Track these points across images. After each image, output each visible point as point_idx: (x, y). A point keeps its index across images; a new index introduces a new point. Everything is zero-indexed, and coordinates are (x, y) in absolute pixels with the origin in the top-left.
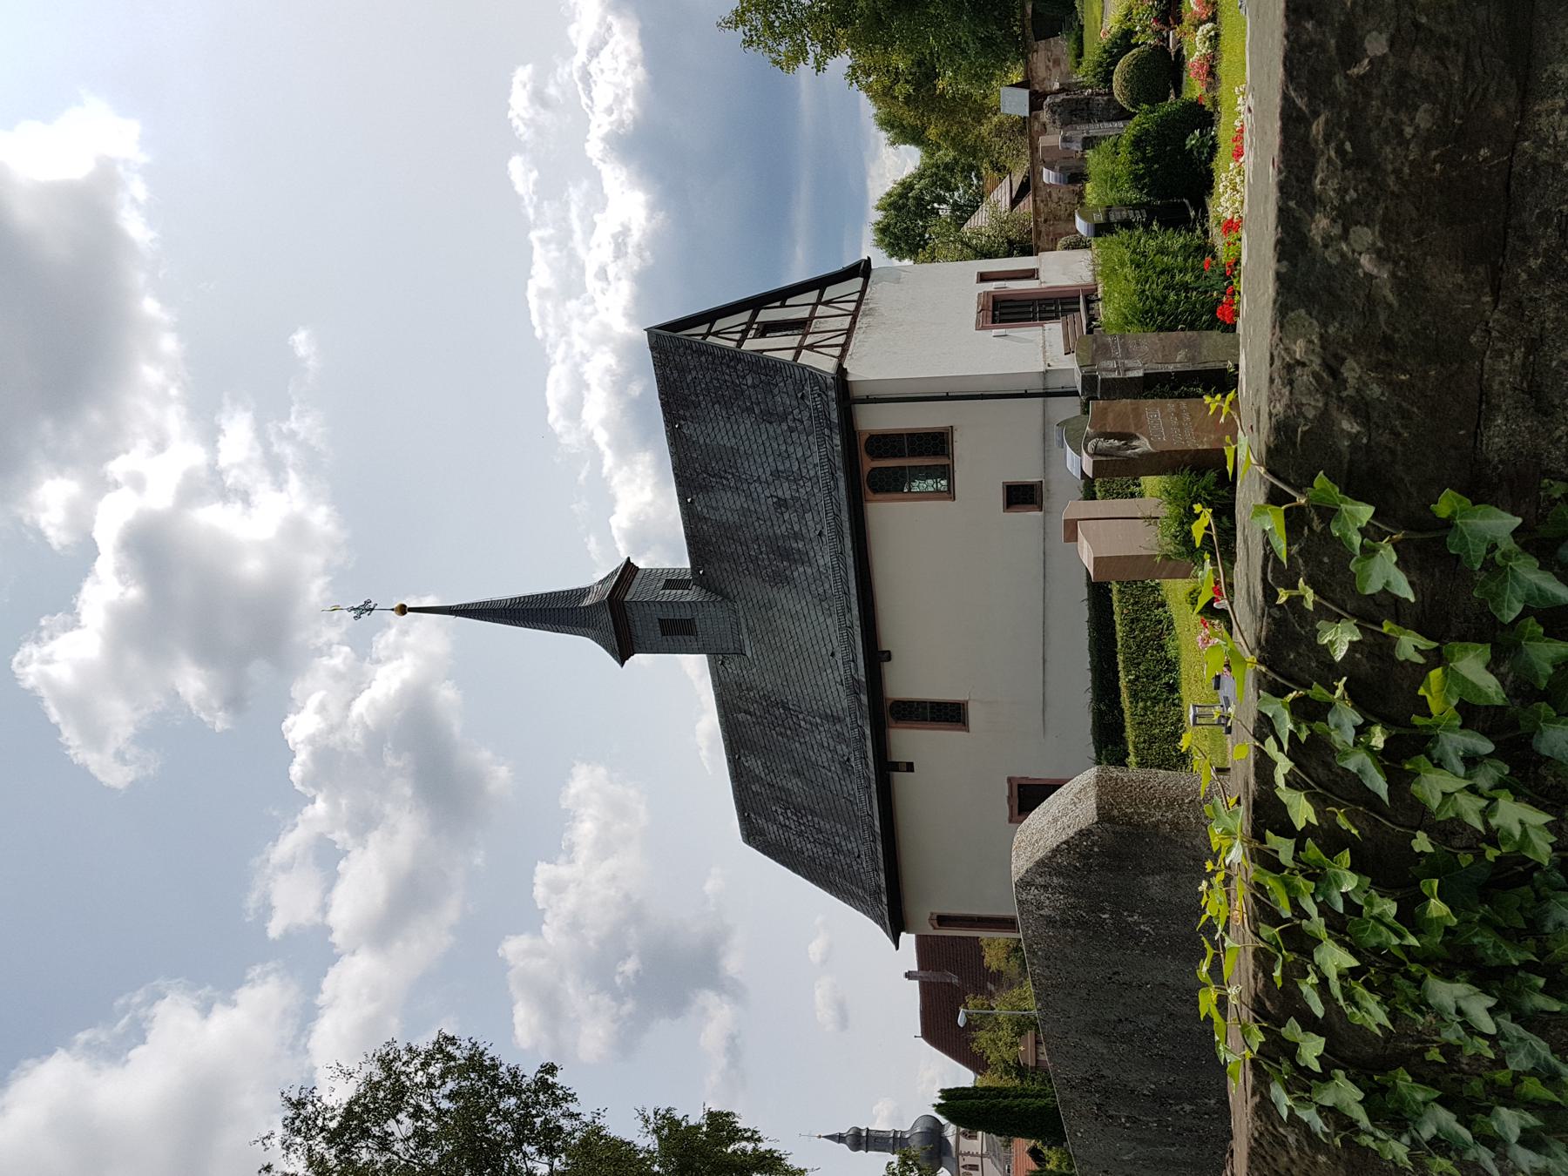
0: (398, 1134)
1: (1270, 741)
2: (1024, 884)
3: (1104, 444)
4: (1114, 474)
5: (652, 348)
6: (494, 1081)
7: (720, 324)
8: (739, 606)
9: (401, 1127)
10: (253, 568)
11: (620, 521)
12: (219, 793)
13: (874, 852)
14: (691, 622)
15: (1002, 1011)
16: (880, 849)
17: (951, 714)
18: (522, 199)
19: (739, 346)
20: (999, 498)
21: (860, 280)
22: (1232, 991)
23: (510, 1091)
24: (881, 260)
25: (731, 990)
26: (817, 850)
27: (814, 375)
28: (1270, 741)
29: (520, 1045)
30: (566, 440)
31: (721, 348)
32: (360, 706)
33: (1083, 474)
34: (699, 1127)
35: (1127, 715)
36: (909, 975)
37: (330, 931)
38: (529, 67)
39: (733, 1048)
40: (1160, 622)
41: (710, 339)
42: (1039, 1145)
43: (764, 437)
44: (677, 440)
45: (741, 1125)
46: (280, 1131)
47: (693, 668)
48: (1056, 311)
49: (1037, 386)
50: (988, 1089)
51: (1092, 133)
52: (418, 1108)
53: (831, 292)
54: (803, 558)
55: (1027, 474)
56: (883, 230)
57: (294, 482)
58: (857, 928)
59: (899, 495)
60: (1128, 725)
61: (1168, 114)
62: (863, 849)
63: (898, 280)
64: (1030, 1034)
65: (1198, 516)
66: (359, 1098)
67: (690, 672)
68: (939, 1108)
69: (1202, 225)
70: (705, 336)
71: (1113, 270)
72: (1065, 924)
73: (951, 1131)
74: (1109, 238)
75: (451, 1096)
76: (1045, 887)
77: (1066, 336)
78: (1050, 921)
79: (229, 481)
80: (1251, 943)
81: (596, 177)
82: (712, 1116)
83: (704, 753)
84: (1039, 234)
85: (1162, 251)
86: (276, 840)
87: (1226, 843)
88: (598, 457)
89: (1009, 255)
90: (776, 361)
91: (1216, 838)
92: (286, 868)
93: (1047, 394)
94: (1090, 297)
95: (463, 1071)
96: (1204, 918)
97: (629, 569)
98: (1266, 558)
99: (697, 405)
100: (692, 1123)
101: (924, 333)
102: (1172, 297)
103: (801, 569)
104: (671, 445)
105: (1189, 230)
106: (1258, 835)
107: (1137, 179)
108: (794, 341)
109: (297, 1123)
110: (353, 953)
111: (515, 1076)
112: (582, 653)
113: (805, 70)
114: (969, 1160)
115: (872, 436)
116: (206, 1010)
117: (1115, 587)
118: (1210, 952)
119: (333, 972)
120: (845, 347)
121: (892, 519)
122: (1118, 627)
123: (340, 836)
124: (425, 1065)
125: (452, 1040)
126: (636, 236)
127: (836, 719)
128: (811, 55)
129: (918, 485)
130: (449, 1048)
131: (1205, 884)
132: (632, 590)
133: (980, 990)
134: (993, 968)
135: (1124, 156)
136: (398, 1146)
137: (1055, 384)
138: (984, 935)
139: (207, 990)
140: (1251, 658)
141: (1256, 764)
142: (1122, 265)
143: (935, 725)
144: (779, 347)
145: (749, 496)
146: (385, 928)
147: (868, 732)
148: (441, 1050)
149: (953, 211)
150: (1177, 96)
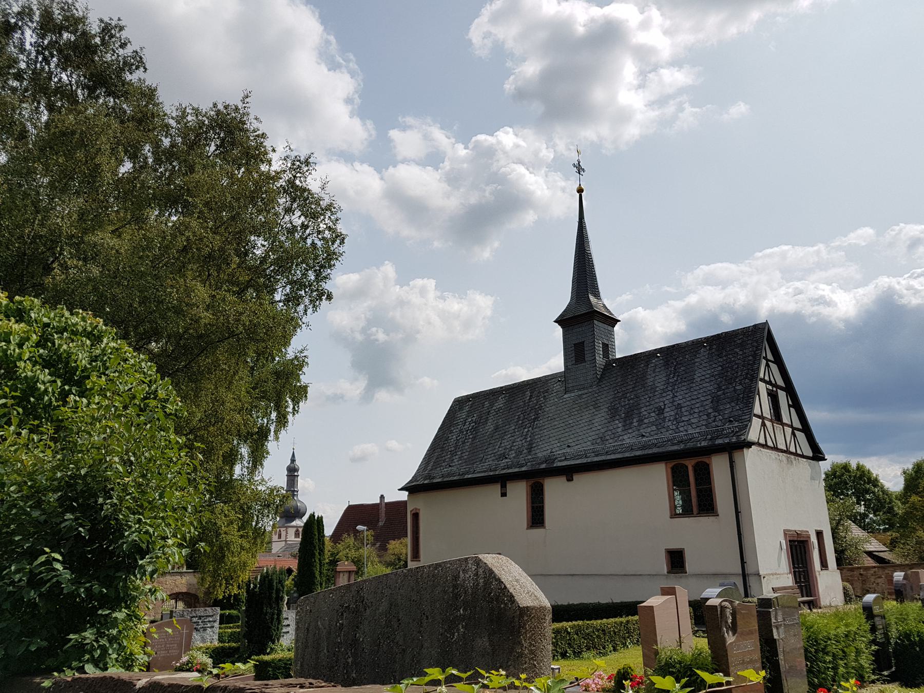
0: (293, 217)
2: (478, 562)
3: (728, 612)
5: (755, 326)
6: (322, 267)
7: (774, 367)
8: (595, 388)
9: (297, 219)
10: (598, 95)
11: (641, 313)
12: (470, 97)
13: (453, 475)
15: (366, 551)
16: (455, 478)
17: (537, 518)
18: (846, 236)
21: (811, 454)
23: (317, 276)
24: (825, 466)
25: (368, 395)
26: (452, 441)
27: (746, 427)
29: (340, 280)
31: (758, 369)
32: (521, 169)
33: (707, 599)
34: (299, 381)
36: (382, 497)
37: (395, 166)
39: (338, 398)
40: (604, 648)
41: (764, 362)
42: (294, 574)
43: (702, 399)
44: (695, 346)
45: (301, 404)
46: (293, 154)
47: (555, 363)
49: (750, 569)
50: (323, 544)
52: (307, 227)
53: (801, 436)
54: (627, 426)
55: (690, 565)
56: (846, 468)
57: (654, 114)
58: (409, 469)
59: (671, 484)
62: (454, 469)
64: (354, 568)
66: (312, 194)
67: (553, 362)
69: (878, 680)
70: (766, 358)
71: (842, 619)
72: (455, 587)
73: (299, 523)
74: (863, 617)
75: (313, 244)
76: (476, 574)
77: (785, 588)
78: (456, 578)
79: (651, 76)
81: (864, 283)
83: (504, 372)
86: (442, 128)
88: (680, 297)
89: (836, 551)
90: (753, 403)
92: (427, 137)
93: (745, 576)
94: (812, 605)
97: (613, 322)
99: (719, 356)
101: (779, 496)
102: (829, 658)
103: (620, 425)
104: (693, 341)
105: (873, 670)
107: (907, 635)
108: (767, 413)
110: (382, 179)
111: (326, 278)
114: (283, 534)
115: (708, 465)
116: (348, 101)
118: (464, 676)
119: (370, 170)
120: (765, 446)
121: (657, 478)
122: (599, 621)
123: (447, 165)
124: (329, 229)
125: (342, 242)
126: (825, 311)
127: (530, 450)
130: (338, 241)
132: (601, 324)
133: (377, 538)
134: (388, 546)
136: (287, 218)
137: (752, 581)
138: (408, 540)
139: (358, 101)
142: (847, 625)
143: (530, 509)
144: (762, 404)
145: (664, 391)
147: (523, 469)
148: (337, 237)
149: (860, 514)
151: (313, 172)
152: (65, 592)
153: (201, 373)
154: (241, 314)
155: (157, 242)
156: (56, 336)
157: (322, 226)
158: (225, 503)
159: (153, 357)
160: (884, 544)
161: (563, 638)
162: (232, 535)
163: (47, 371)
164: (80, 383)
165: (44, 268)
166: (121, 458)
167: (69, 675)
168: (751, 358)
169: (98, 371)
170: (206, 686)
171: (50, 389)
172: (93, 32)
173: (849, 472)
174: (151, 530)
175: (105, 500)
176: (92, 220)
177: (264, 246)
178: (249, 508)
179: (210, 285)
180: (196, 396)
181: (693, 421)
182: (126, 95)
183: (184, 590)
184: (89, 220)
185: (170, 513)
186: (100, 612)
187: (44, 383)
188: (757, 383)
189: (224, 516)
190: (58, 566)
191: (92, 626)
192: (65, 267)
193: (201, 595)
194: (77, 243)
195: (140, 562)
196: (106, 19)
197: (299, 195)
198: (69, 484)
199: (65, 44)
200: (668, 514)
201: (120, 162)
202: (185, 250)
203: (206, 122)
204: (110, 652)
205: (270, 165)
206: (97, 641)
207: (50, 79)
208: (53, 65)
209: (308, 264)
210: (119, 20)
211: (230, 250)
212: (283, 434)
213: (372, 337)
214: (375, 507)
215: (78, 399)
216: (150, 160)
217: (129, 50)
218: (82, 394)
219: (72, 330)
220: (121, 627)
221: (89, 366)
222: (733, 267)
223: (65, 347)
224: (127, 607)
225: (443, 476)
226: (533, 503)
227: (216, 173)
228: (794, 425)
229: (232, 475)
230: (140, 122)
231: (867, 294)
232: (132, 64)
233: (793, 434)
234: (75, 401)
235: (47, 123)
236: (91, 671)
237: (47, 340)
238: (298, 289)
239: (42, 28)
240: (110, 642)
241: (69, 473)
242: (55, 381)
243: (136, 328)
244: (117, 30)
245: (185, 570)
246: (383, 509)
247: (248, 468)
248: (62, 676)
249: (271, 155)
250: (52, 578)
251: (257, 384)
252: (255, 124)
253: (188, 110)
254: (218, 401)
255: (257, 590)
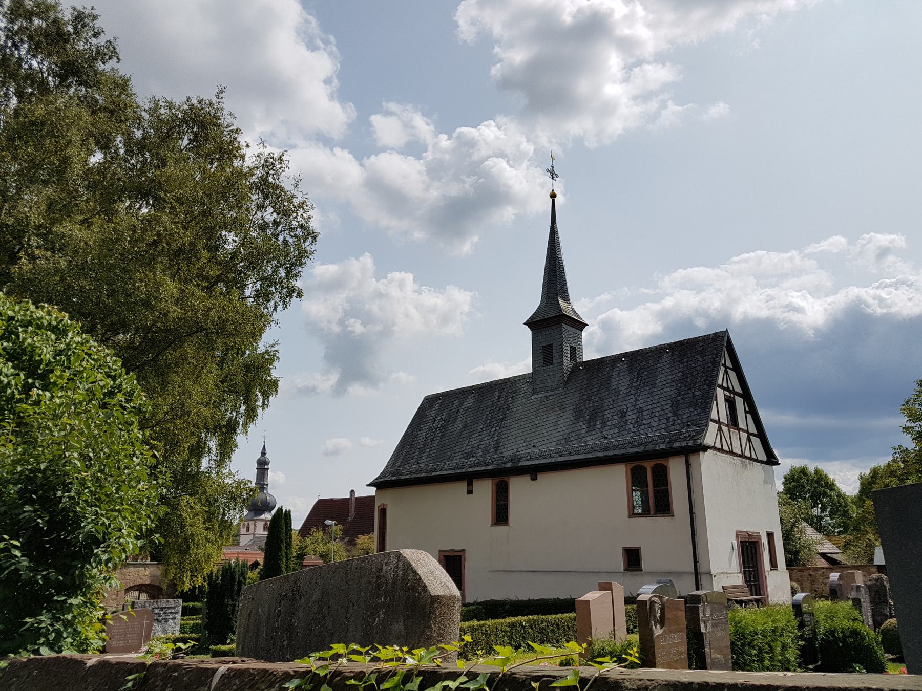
1: (466, 679)
2: (399, 556)
3: (657, 607)
4: (641, 615)
5: (715, 334)
6: (293, 264)
7: (732, 374)
8: (561, 390)
9: (269, 215)
10: (583, 86)
13: (421, 472)
14: (552, 363)
17: (501, 516)
19: (720, 386)
20: (631, 544)
21: (765, 459)
22: (344, 661)
25: (340, 389)
26: (421, 439)
27: (702, 431)
28: (466, 679)
29: (316, 272)
30: (667, 279)
31: (717, 375)
32: (503, 163)
34: (269, 375)
35: (502, 621)
36: (352, 492)
37: (376, 155)
38: (904, 244)
39: (309, 391)
40: (558, 642)
41: (722, 369)
42: (260, 567)
44: (659, 351)
45: (271, 398)
48: (750, 581)
49: (701, 569)
50: (291, 538)
51: (864, 605)
53: (756, 441)
54: (591, 428)
56: (803, 471)
57: (637, 110)
58: (377, 466)
60: (496, 621)
61: (876, 653)
62: (422, 466)
63: (765, 482)
65: (580, 645)
68: (280, 509)
70: (724, 365)
72: (378, 578)
73: (268, 516)
74: (792, 614)
75: (285, 241)
76: (397, 567)
77: (734, 587)
78: (379, 570)
79: (636, 70)
80: (368, 671)
81: (834, 292)
82: (275, 383)
84: (801, 571)
85: (784, 647)
86: (423, 115)
87: (416, 657)
88: (658, 299)
90: (710, 409)
91: (421, 652)
92: (408, 126)
93: (697, 575)
95: (298, 246)
96: (380, 647)
97: (581, 326)
98: (555, 677)
100: (272, 371)
101: (733, 498)
102: (754, 652)
103: (584, 427)
104: (656, 347)
106: (420, 673)
107: (832, 632)
108: (724, 419)
109: (271, 160)
110: (361, 165)
111: (296, 276)
112: (532, 301)
113: (904, 421)
114: (252, 527)
115: (666, 467)
116: (327, 81)
117: (573, 615)
120: (721, 450)
121: (614, 482)
122: (554, 616)
123: (429, 155)
125: (314, 239)
126: (795, 317)
127: (496, 449)
128: (913, 425)
129: (637, 495)
130: (310, 239)
131: (397, 648)
132: (569, 328)
133: (345, 533)
134: (357, 541)
135: (847, 624)
136: (259, 214)
137: (704, 580)
138: (375, 535)
140: (506, 669)
141: (454, 672)
142: (774, 621)
143: (495, 506)
144: (719, 410)
145: (627, 394)
146: (377, 186)
147: (490, 467)
148: (309, 235)
150: (890, 660)
151: (286, 169)
152: (23, 578)
153: (168, 366)
154: (210, 309)
155: (127, 234)
156: (20, 329)
157: (295, 223)
158: (191, 495)
159: (120, 351)
160: (838, 547)
161: (517, 632)
162: (196, 526)
163: (10, 364)
164: (44, 377)
165: (9, 257)
166: (80, 454)
167: (25, 656)
168: (710, 365)
169: (62, 365)
170: (149, 662)
171: (13, 383)
172: (66, 19)
173: (807, 475)
174: (107, 522)
175: (63, 493)
176: (61, 210)
177: (235, 241)
178: (216, 500)
179: (179, 279)
180: (163, 389)
181: (653, 424)
182: (97, 85)
183: (148, 582)
184: (58, 210)
185: (126, 506)
186: (55, 598)
187: (7, 376)
188: (715, 389)
189: (190, 510)
190: (17, 553)
191: (49, 611)
192: (33, 258)
193: (165, 587)
194: (44, 233)
195: (95, 551)
196: (79, 8)
197: (270, 190)
198: (30, 478)
199: (36, 30)
200: (626, 513)
201: (91, 153)
202: (155, 243)
203: (180, 116)
204: (65, 635)
205: (243, 160)
206: (52, 625)
207: (20, 66)
208: (23, 52)
209: (279, 260)
210: (93, 8)
211: (200, 245)
212: (252, 428)
213: (349, 329)
214: (344, 502)
215: (41, 392)
216: (122, 151)
217: (102, 40)
218: (45, 388)
219: (37, 324)
220: (75, 613)
221: (53, 360)
222: (709, 270)
223: (29, 341)
224: (84, 595)
225: (411, 473)
226: (498, 501)
227: (188, 170)
228: (750, 431)
229: (198, 468)
230: (112, 112)
231: (841, 299)
232: (105, 55)
233: (749, 439)
234: (38, 395)
235: (16, 110)
236: (45, 652)
237: (11, 333)
238: (267, 286)
239: (12, 13)
240: (65, 627)
241: (29, 467)
242: (18, 375)
243: (99, 320)
244: (91, 18)
245: (148, 562)
246: (354, 504)
247: (215, 460)
248: (18, 657)
249: (244, 151)
250: (10, 566)
251: (226, 377)
252: (229, 120)
253: (161, 103)
254: (185, 393)
255: (219, 582)
